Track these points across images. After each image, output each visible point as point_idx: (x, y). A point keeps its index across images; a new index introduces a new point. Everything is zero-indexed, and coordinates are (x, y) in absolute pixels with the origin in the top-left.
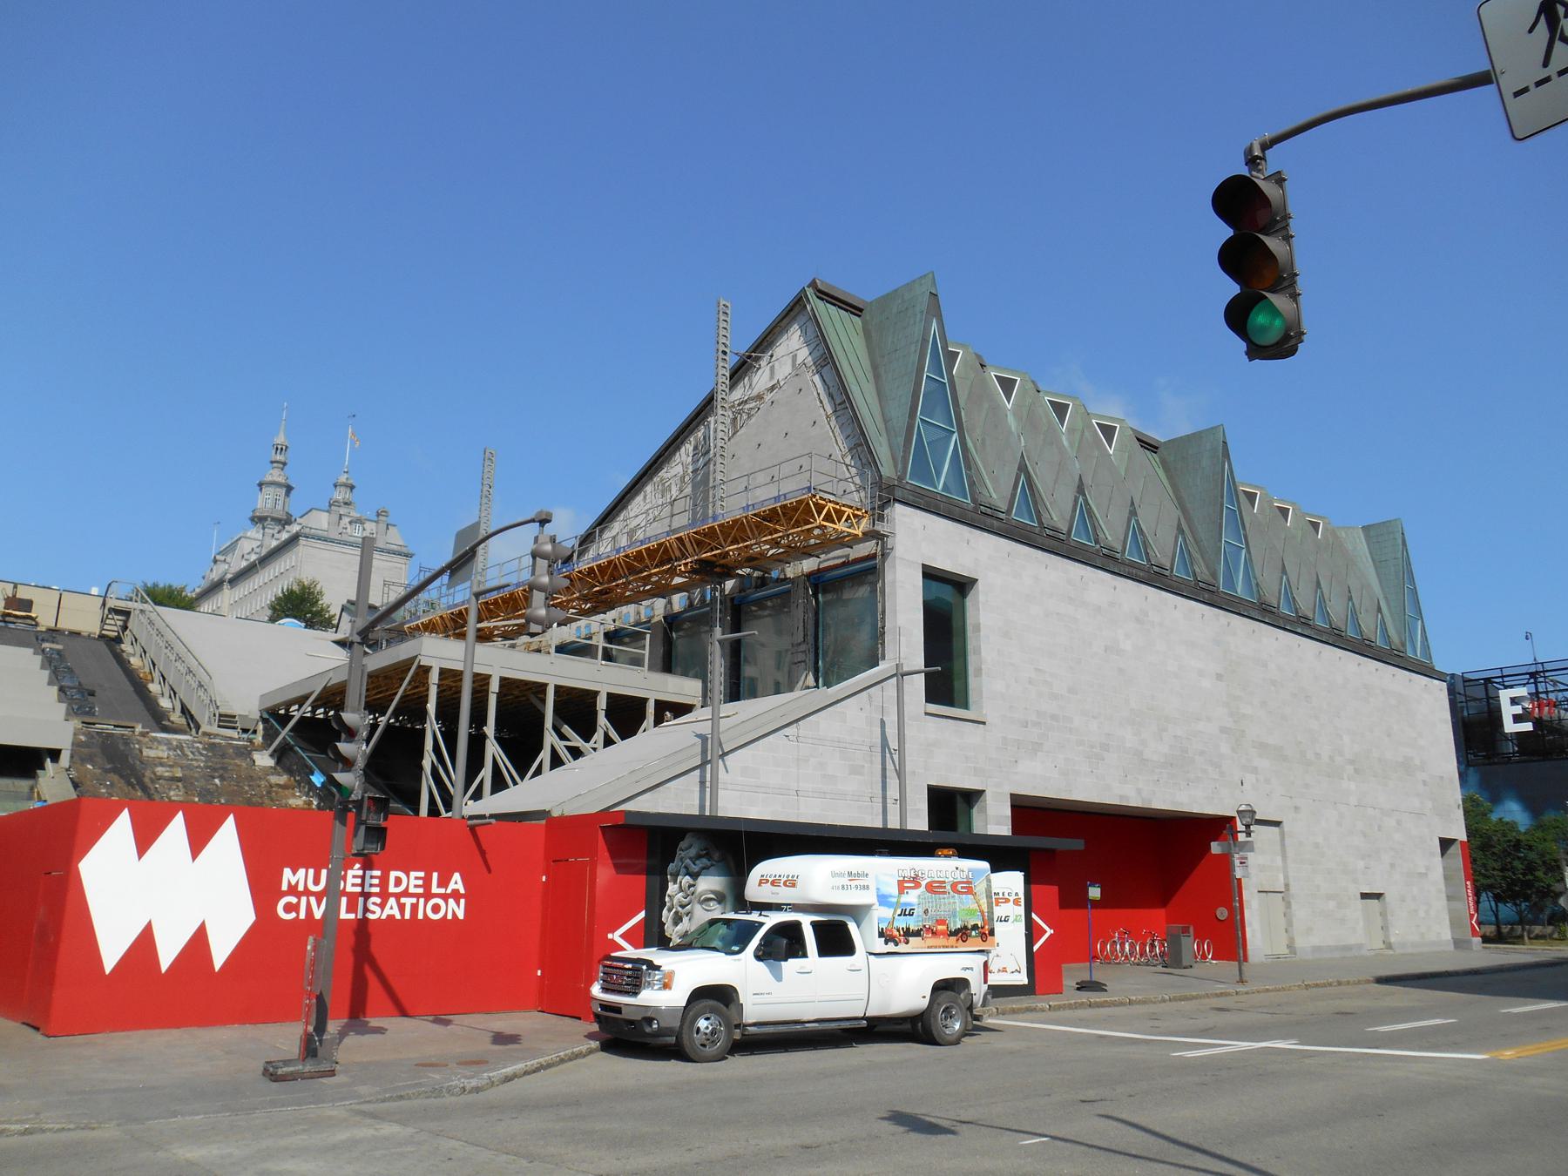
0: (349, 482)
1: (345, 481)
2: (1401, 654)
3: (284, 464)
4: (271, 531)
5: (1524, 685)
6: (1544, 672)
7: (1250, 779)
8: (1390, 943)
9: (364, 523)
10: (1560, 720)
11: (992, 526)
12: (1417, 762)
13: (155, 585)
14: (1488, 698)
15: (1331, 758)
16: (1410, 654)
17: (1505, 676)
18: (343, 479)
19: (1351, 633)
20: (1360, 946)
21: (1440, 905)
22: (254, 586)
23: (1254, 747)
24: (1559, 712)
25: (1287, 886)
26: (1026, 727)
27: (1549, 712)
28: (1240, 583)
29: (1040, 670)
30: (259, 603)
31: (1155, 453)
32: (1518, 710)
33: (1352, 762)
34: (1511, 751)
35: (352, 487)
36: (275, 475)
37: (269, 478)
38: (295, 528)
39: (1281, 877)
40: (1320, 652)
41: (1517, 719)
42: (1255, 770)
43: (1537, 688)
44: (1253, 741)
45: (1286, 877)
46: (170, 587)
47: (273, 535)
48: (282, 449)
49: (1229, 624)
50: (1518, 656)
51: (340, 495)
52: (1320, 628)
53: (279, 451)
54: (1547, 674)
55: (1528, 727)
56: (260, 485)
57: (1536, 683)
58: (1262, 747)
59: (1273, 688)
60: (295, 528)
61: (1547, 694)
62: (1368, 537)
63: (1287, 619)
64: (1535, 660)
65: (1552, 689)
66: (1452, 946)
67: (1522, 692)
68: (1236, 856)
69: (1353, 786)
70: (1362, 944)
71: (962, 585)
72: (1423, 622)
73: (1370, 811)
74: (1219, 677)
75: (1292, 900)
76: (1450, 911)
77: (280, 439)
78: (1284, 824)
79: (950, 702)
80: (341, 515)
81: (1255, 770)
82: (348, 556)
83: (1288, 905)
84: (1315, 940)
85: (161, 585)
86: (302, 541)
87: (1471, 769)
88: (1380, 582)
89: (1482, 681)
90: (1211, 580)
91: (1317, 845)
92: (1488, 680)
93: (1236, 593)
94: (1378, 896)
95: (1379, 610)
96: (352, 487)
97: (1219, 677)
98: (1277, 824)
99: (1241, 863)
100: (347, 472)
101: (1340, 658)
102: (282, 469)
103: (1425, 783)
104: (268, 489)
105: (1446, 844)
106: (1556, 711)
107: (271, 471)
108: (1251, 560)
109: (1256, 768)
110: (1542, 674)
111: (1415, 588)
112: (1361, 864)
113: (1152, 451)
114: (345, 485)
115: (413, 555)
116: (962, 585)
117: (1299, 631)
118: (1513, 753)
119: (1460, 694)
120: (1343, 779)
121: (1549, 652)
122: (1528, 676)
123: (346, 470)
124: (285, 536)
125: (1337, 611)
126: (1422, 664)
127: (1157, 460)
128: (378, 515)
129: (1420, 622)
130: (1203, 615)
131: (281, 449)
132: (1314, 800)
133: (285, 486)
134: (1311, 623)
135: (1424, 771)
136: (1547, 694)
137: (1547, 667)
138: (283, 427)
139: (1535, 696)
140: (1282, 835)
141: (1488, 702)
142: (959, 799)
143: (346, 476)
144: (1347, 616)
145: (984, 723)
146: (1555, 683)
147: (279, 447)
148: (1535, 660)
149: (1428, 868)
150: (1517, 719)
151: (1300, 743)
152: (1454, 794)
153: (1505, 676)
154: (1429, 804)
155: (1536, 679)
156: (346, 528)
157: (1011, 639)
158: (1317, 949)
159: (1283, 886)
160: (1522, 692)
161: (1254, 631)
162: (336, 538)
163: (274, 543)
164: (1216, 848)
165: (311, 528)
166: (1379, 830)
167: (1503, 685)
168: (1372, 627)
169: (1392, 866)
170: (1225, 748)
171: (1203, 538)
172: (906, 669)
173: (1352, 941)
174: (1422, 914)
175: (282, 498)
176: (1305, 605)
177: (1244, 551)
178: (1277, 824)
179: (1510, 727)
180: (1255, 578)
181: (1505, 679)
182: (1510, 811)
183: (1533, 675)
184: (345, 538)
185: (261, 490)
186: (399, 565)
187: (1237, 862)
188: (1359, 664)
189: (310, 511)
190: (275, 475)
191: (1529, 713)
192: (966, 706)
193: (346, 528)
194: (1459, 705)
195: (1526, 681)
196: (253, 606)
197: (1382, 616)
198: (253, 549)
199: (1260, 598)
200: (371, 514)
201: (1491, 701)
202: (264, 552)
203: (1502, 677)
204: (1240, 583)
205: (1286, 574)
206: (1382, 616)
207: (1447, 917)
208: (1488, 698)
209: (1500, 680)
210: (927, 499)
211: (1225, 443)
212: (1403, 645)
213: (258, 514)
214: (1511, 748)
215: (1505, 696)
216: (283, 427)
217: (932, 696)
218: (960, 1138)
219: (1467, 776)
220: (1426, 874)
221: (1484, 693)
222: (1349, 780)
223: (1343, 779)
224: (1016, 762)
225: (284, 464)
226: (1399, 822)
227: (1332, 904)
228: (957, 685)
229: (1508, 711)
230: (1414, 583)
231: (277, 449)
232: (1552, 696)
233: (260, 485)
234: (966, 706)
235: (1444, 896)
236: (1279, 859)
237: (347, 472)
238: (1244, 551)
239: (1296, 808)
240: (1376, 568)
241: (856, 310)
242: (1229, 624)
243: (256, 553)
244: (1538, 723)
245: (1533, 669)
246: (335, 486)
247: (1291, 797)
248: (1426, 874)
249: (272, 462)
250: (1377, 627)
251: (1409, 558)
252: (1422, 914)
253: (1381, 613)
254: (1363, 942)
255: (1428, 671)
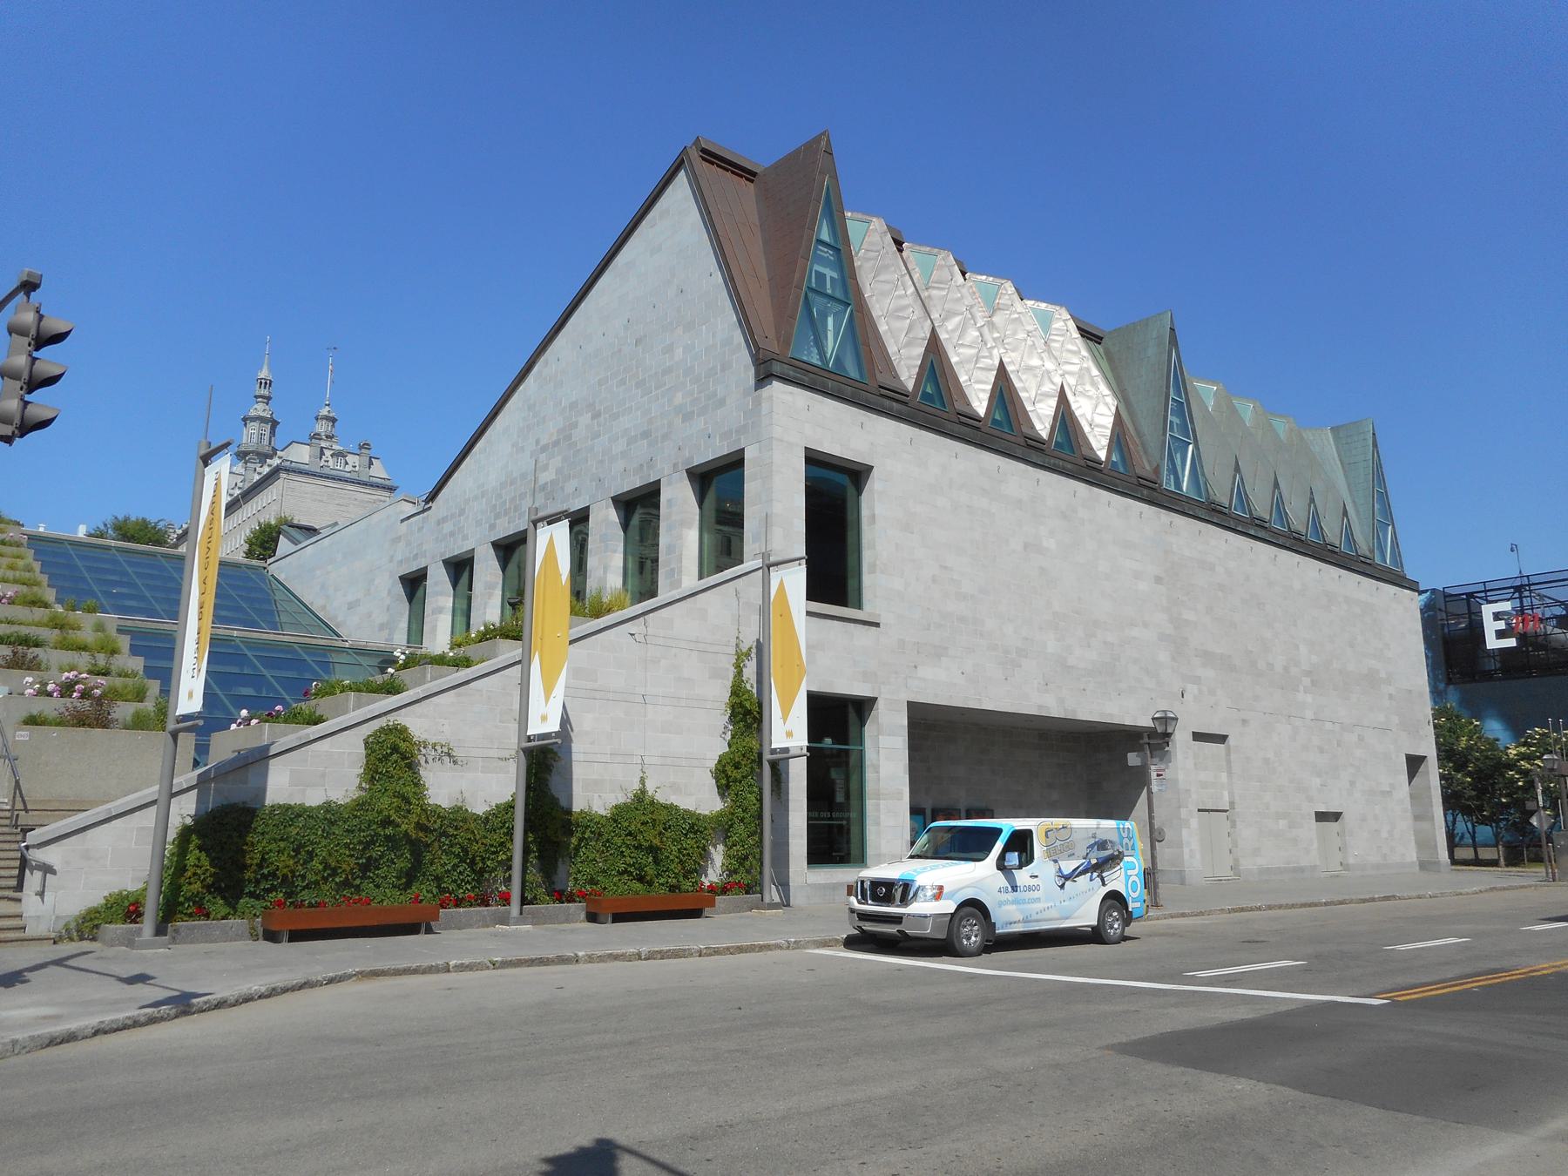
0: (331, 415)
1: (326, 413)
2: (1368, 561)
3: (269, 398)
4: (253, 466)
5: (1508, 600)
6: (1529, 585)
7: (1191, 689)
8: (1348, 865)
9: (346, 456)
10: (1546, 635)
11: (891, 410)
12: (1383, 675)
13: (127, 519)
14: (1470, 613)
15: (1286, 669)
16: (1378, 560)
17: (1489, 591)
18: (324, 412)
19: (1311, 538)
20: (1314, 868)
21: (1405, 825)
22: (238, 521)
23: (1196, 656)
24: (1545, 627)
25: (1232, 804)
26: (928, 629)
27: (1534, 626)
28: (1186, 479)
29: (946, 568)
30: (238, 541)
31: (1100, 343)
32: (1501, 625)
33: (1308, 673)
34: (1493, 668)
35: (333, 420)
36: (259, 409)
37: (252, 413)
38: (276, 462)
39: (1226, 794)
40: (1276, 556)
41: (1501, 634)
42: (1197, 680)
43: (1521, 602)
44: (1196, 649)
45: (1231, 794)
46: (144, 520)
47: (255, 470)
48: (266, 383)
49: (1171, 523)
50: (1504, 569)
51: (322, 428)
52: (1278, 532)
53: (263, 385)
54: (1532, 588)
55: (1511, 642)
56: (245, 420)
57: (1521, 598)
58: (1207, 657)
59: (1220, 594)
60: (276, 462)
61: (1532, 609)
62: (1337, 439)
63: (1238, 519)
64: (1520, 572)
65: (1538, 602)
66: (1418, 868)
67: (1506, 606)
68: (1153, 767)
69: (1309, 699)
70: (1315, 866)
71: (857, 474)
72: (1393, 527)
73: (1328, 726)
74: (1158, 580)
75: (1237, 820)
76: (1416, 833)
77: (264, 373)
78: (1231, 741)
79: (842, 601)
80: (322, 448)
81: (1197, 680)
82: (331, 489)
83: (1234, 825)
84: (1262, 861)
85: (133, 519)
86: (283, 475)
87: (1451, 687)
88: (1349, 486)
89: (1465, 597)
90: (1153, 477)
91: (1266, 761)
92: (1470, 595)
93: (1182, 491)
94: (1336, 816)
95: (1345, 513)
96: (333, 420)
97: (1158, 580)
98: (1222, 739)
99: (1158, 775)
100: (328, 405)
101: (1298, 563)
102: (267, 404)
103: (1391, 696)
104: (252, 423)
105: (1414, 763)
106: (1542, 626)
107: (256, 406)
108: (1199, 456)
109: (1200, 677)
110: (1527, 588)
111: (1386, 492)
112: (1317, 781)
113: (1096, 342)
114: (327, 418)
115: (397, 487)
116: (857, 474)
117: (1252, 532)
118: (1496, 670)
119: (1440, 610)
120: (1298, 691)
121: (1534, 564)
122: (1512, 590)
123: (327, 403)
124: (266, 470)
125: (1298, 519)
126: (1390, 571)
127: (1101, 350)
128: (361, 447)
129: (1390, 528)
130: (1141, 513)
131: (267, 384)
132: (1265, 713)
133: (271, 422)
134: (1267, 525)
135: (1390, 685)
136: (1532, 609)
137: (1534, 580)
138: (266, 362)
139: (1521, 611)
140: (1228, 750)
141: (1470, 617)
142: (851, 710)
143: (327, 408)
144: (1309, 518)
145: (877, 625)
146: (1542, 597)
147: (263, 381)
148: (1520, 572)
149: (1392, 786)
150: (1501, 634)
151: (1251, 652)
152: (1425, 708)
153: (1489, 591)
154: (1395, 720)
155: (1521, 593)
156: (328, 461)
157: (913, 533)
158: (1264, 871)
159: (1228, 804)
160: (1506, 606)
161: (1200, 532)
162: (318, 471)
163: (257, 477)
164: (1133, 759)
165: (292, 462)
166: (1339, 745)
167: (1486, 600)
168: (1337, 531)
169: (1352, 783)
170: (1163, 657)
171: (1146, 433)
172: (773, 559)
173: (1304, 863)
174: (1384, 834)
175: (267, 433)
176: (1261, 507)
177: (1191, 447)
178: (1222, 739)
179: (1492, 643)
180: (1203, 475)
181: (1488, 594)
182: (1492, 730)
183: (1518, 589)
184: (326, 471)
185: (245, 425)
186: (383, 498)
187: (1154, 775)
188: (1320, 570)
189: (291, 444)
190: (259, 409)
191: (1513, 628)
192: (859, 606)
193: (328, 461)
194: (1440, 622)
195: (1509, 596)
196: (238, 541)
197: (1348, 520)
198: (236, 485)
199: (1208, 498)
200: (353, 447)
201: (1473, 617)
202: (247, 485)
203: (1486, 591)
204: (1186, 479)
205: (1240, 473)
206: (1348, 520)
207: (1413, 838)
208: (1470, 613)
209: (1483, 594)
210: (812, 375)
211: (1172, 329)
212: (1372, 551)
213: (243, 449)
214: (1492, 665)
215: (1487, 611)
216: (266, 362)
217: (813, 594)
218: (536, 1153)
219: (1446, 694)
220: (1389, 793)
221: (1466, 607)
222: (1305, 692)
223: (1298, 691)
224: (916, 667)
225: (269, 398)
226: (1361, 738)
227: (1282, 824)
228: (851, 583)
229: (1491, 627)
230: (1385, 487)
231: (261, 383)
232: (1539, 612)
233: (245, 420)
234: (859, 606)
235: (1409, 814)
236: (1224, 775)
237: (328, 405)
238: (1191, 447)
239: (1244, 722)
240: (1345, 471)
241: (748, 174)
242: (1171, 523)
243: (239, 488)
244: (1522, 638)
245: (1518, 583)
246: (317, 419)
247: (1239, 710)
248: (1389, 793)
249: (256, 397)
250: (1342, 531)
251: (1380, 460)
252: (1384, 834)
253: (1347, 517)
254: (1318, 863)
255: (1397, 579)
